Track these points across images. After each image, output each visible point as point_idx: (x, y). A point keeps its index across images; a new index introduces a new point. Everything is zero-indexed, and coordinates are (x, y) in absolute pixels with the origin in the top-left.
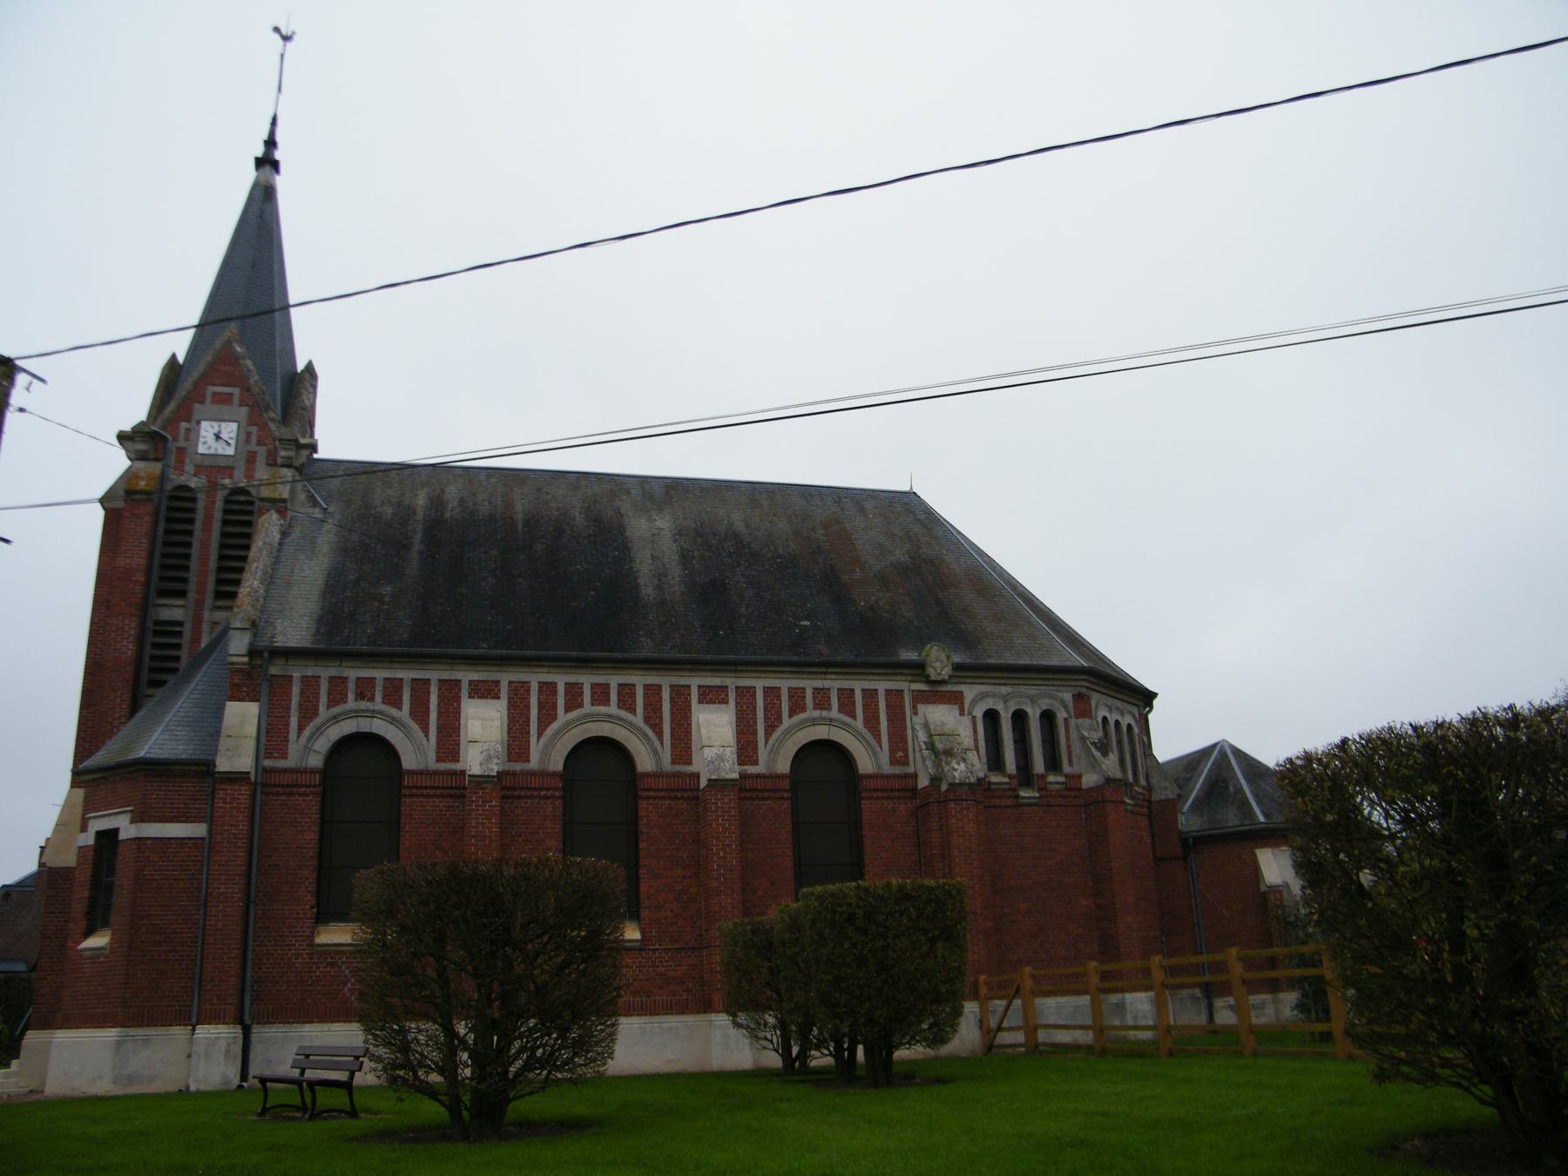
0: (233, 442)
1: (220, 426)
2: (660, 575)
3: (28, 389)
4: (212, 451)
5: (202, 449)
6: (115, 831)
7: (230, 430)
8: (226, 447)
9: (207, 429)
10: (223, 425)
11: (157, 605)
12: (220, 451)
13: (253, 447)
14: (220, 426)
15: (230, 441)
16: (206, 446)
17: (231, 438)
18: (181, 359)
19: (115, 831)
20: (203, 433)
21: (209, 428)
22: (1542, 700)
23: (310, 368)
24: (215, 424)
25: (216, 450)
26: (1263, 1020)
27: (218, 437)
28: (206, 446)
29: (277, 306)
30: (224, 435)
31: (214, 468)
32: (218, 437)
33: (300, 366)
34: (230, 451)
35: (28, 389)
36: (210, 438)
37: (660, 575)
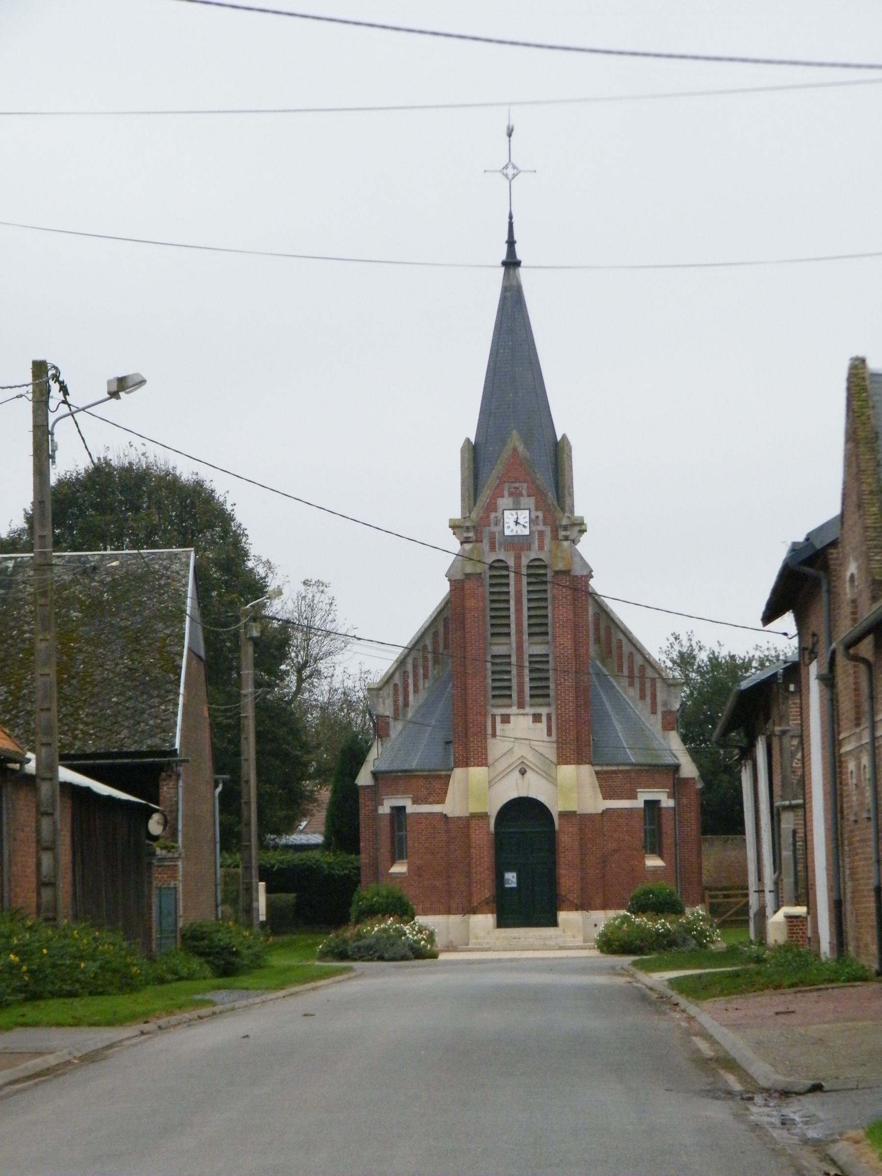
0: (527, 525)
1: (517, 514)
2: (745, 769)
3: (485, 171)
4: (514, 533)
5: (507, 532)
6: (404, 808)
7: (524, 516)
8: (523, 529)
9: (509, 517)
10: (519, 512)
11: (491, 644)
12: (520, 533)
13: (541, 527)
14: (517, 514)
15: (526, 525)
16: (510, 530)
17: (526, 522)
18: (473, 440)
19: (404, 808)
20: (506, 520)
21: (510, 516)
22: (25, 510)
23: (564, 437)
24: (514, 512)
25: (517, 532)
26: (515, 880)
27: (517, 523)
28: (510, 530)
29: (460, 558)
30: (521, 521)
31: (518, 544)
32: (517, 523)
33: (559, 438)
34: (526, 532)
35: (485, 171)
36: (512, 525)
37: (745, 769)
